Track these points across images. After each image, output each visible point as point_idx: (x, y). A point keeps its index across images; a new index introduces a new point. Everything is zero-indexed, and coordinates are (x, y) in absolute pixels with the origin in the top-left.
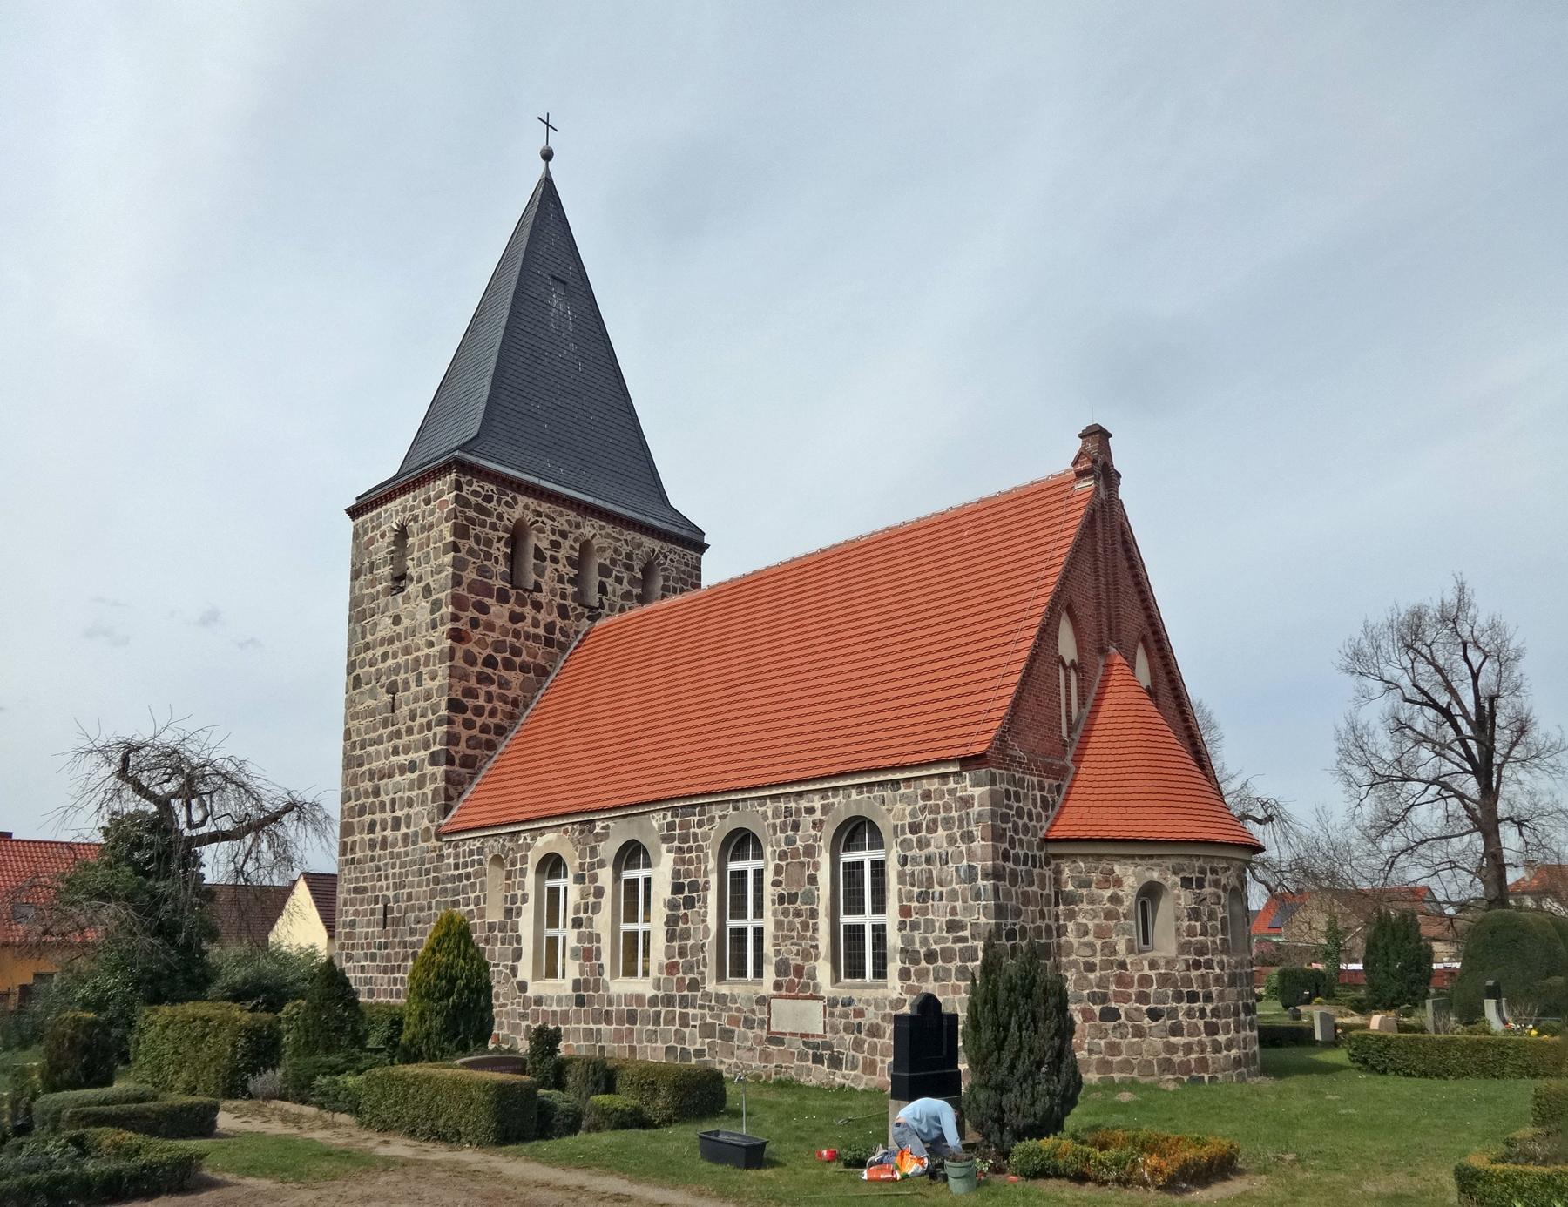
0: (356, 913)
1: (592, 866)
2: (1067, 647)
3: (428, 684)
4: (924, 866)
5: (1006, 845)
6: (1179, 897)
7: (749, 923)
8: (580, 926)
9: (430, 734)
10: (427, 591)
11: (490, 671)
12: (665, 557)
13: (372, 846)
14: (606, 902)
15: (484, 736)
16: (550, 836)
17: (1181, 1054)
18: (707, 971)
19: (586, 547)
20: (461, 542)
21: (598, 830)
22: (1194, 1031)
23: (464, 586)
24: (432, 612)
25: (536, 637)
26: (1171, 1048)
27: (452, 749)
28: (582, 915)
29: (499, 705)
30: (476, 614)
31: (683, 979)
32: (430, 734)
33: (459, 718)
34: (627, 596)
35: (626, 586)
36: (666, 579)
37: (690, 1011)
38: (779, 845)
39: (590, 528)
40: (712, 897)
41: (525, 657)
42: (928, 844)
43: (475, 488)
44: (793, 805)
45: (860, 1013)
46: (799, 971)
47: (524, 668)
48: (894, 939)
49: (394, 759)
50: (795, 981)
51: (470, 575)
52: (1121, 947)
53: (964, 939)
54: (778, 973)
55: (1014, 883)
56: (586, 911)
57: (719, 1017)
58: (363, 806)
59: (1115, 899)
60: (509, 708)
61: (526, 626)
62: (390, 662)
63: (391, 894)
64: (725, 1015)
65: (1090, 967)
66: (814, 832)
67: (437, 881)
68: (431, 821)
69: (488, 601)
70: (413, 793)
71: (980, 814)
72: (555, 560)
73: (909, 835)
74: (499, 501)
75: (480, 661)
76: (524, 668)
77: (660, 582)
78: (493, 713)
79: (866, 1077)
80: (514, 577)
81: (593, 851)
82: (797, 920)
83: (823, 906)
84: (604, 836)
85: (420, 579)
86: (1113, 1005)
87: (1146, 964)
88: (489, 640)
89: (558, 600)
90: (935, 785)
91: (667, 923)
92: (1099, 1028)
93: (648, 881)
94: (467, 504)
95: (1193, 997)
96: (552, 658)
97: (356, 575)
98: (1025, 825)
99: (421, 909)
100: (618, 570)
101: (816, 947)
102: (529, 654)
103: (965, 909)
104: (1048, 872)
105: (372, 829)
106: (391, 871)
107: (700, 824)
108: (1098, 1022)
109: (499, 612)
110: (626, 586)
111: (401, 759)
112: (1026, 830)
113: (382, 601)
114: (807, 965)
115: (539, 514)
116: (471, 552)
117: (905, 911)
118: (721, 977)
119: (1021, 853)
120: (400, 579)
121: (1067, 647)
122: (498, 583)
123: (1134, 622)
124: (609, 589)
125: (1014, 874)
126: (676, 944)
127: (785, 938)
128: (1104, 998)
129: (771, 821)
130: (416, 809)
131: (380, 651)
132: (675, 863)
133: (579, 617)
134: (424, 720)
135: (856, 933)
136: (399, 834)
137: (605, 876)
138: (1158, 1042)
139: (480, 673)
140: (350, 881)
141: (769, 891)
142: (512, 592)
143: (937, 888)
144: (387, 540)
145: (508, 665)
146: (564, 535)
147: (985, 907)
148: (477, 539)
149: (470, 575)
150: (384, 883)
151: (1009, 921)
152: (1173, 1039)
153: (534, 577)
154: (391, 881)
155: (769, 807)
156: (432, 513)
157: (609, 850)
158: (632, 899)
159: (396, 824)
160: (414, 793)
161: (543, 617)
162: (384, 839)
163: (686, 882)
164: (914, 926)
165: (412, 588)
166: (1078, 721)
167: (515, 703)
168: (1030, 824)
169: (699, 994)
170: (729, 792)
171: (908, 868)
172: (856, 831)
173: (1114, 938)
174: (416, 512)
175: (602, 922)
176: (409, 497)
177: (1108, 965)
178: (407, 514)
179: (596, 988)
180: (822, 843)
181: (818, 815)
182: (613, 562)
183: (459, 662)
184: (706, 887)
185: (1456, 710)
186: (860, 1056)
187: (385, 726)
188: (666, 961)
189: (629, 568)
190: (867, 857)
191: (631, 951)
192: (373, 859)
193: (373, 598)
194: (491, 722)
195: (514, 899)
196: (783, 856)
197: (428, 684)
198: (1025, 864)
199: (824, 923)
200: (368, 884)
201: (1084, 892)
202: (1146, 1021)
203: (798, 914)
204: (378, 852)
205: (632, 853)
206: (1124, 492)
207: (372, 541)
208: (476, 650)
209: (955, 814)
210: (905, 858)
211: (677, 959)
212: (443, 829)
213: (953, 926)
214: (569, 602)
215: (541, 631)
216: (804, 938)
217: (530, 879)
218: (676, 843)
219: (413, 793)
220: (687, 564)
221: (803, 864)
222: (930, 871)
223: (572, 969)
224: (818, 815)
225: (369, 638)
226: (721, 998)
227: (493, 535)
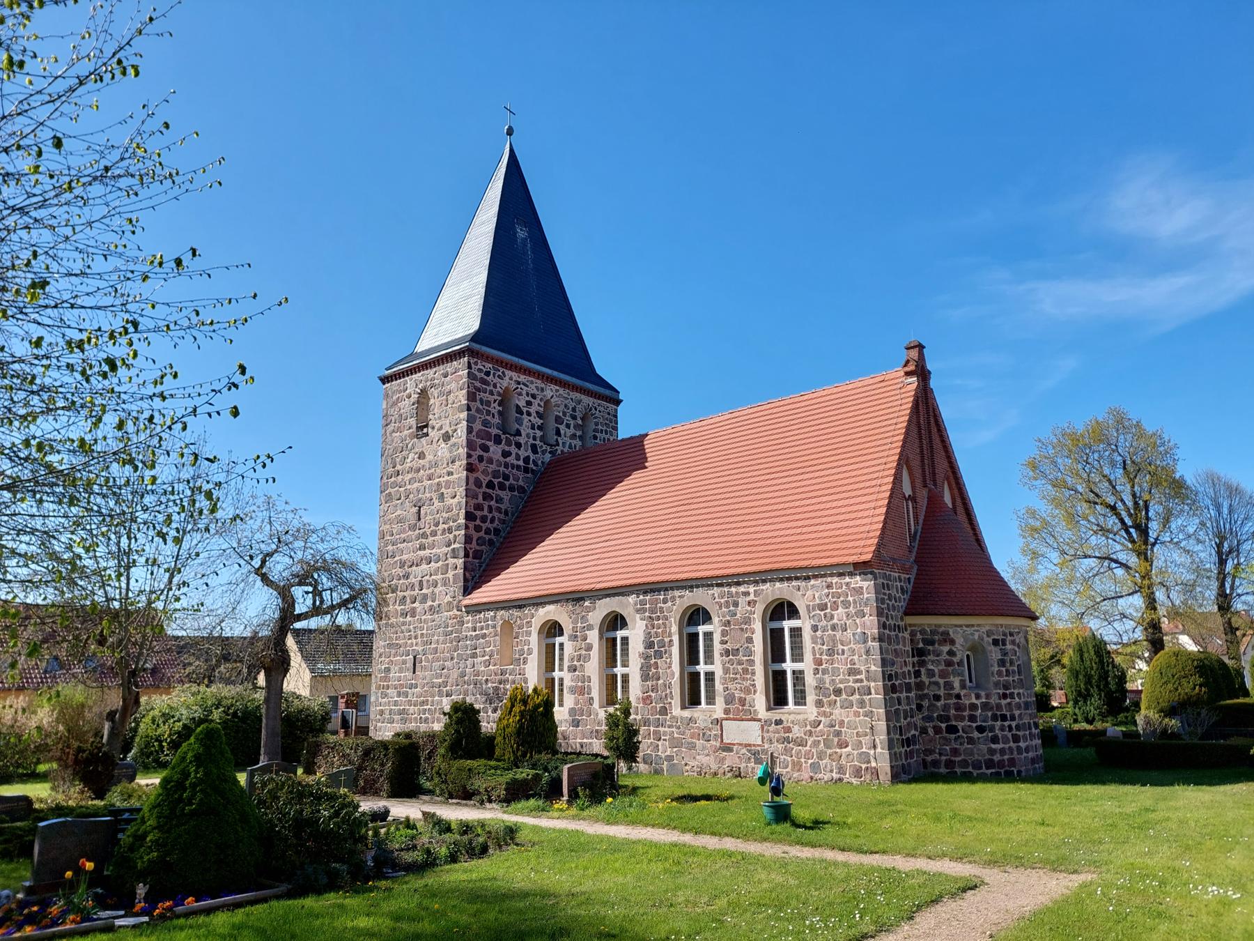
9: (451, 536)
11: (490, 491)
14: (595, 654)
15: (487, 537)
22: (1006, 741)
25: (518, 467)
26: (992, 752)
27: (468, 546)
29: (496, 514)
30: (482, 453)
32: (451, 536)
33: (471, 525)
35: (572, 430)
36: (597, 424)
40: (675, 650)
45: (789, 730)
46: (742, 702)
47: (512, 489)
48: (810, 680)
49: (422, 553)
50: (739, 710)
52: (957, 685)
53: (861, 681)
54: (727, 703)
55: (890, 644)
56: (579, 660)
59: (951, 653)
60: (502, 516)
63: (420, 649)
65: (937, 698)
72: (529, 414)
76: (512, 489)
78: (492, 521)
80: (504, 428)
82: (739, 667)
88: (490, 470)
89: (531, 441)
90: (835, 580)
92: (945, 738)
95: (1004, 718)
101: (754, 685)
107: (665, 601)
108: (945, 734)
109: (495, 451)
110: (572, 430)
111: (427, 552)
115: (519, 383)
117: (818, 662)
118: (683, 707)
120: (422, 429)
122: (494, 431)
123: (941, 465)
128: (947, 719)
134: (446, 526)
137: (593, 636)
138: (984, 748)
139: (484, 493)
141: (717, 647)
144: (412, 400)
146: (534, 396)
149: (478, 426)
152: (993, 746)
161: (523, 453)
164: (825, 672)
166: (916, 533)
171: (819, 633)
173: (952, 678)
177: (949, 696)
181: (752, 597)
185: (1120, 505)
189: (574, 418)
199: (759, 668)
201: (930, 648)
202: (976, 734)
203: (740, 663)
204: (409, 618)
206: (933, 384)
208: (482, 477)
209: (850, 599)
213: (852, 672)
214: (538, 442)
215: (521, 463)
217: (534, 638)
225: (399, 467)
227: (491, 398)
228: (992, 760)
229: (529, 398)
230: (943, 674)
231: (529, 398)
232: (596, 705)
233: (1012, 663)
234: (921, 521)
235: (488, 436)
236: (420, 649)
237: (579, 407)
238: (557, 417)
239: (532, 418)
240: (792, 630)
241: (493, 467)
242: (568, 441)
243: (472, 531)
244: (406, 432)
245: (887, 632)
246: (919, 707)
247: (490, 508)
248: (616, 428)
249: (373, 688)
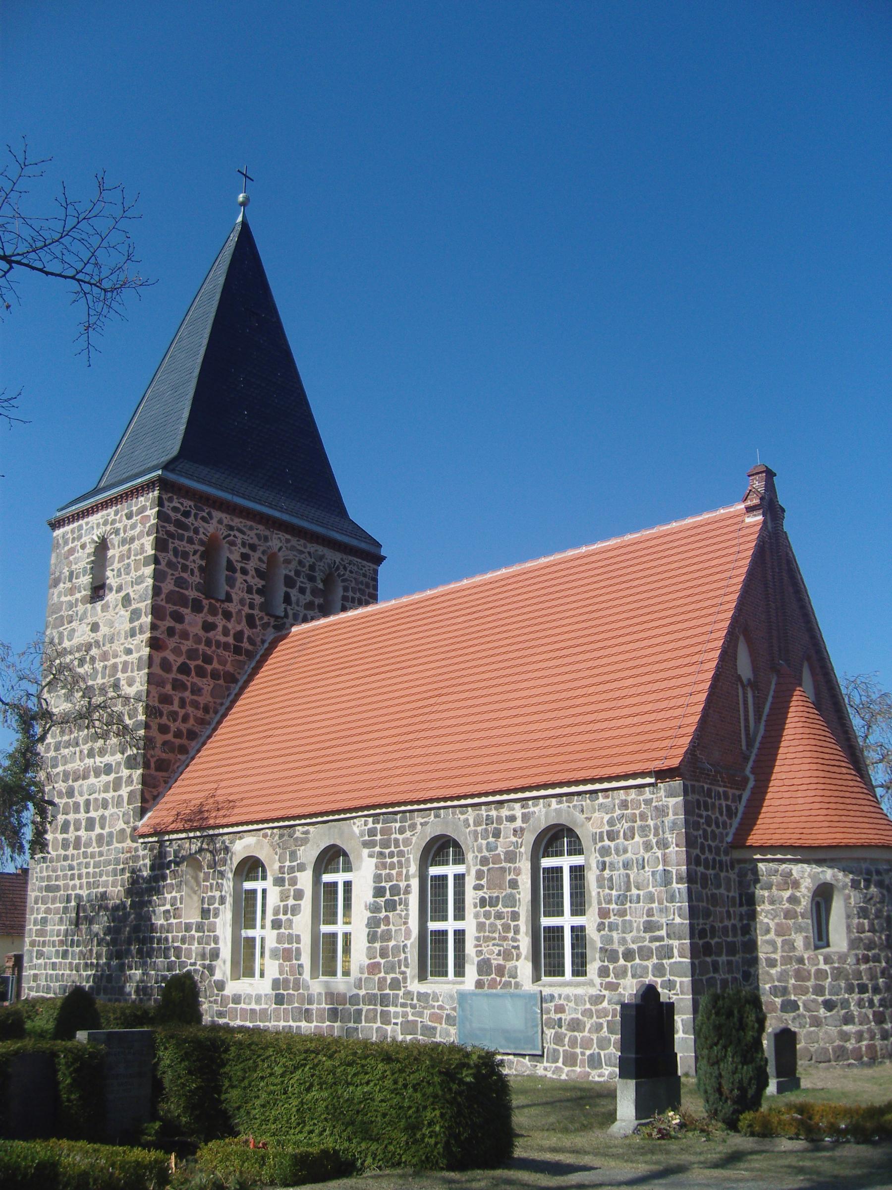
1: (292, 870)
4: (622, 871)
5: (698, 851)
6: (849, 897)
7: (450, 925)
8: (279, 927)
12: (345, 568)
13: (65, 845)
14: (306, 904)
15: (178, 741)
17: (853, 1041)
18: (408, 971)
19: (272, 559)
20: (161, 555)
21: (298, 834)
22: (864, 1020)
23: (163, 596)
24: (131, 621)
25: (226, 646)
26: (845, 1036)
28: (281, 917)
29: (190, 710)
31: (385, 979)
34: (309, 606)
35: (308, 597)
36: (346, 589)
37: (392, 1009)
38: (480, 850)
39: (277, 541)
42: (625, 851)
44: (494, 813)
46: (500, 971)
47: (215, 675)
49: (89, 762)
53: (661, 939)
54: (480, 972)
55: (704, 886)
57: (421, 1015)
59: (793, 900)
60: (200, 714)
61: (217, 635)
64: (427, 1012)
66: (514, 839)
68: (127, 823)
70: (109, 796)
71: (674, 823)
72: (244, 572)
73: (607, 842)
74: (196, 516)
75: (175, 668)
76: (215, 675)
77: (340, 592)
78: (185, 719)
79: (566, 1069)
80: (208, 588)
81: (293, 856)
82: (499, 923)
83: (524, 909)
84: (304, 841)
85: (119, 589)
86: (793, 997)
87: (821, 958)
88: (184, 649)
89: (246, 610)
90: (633, 794)
91: (368, 925)
93: (348, 885)
96: (240, 665)
98: (713, 831)
100: (301, 581)
101: (517, 948)
102: (220, 663)
103: (661, 910)
106: (84, 871)
107: (402, 831)
108: (779, 1013)
109: (193, 622)
110: (308, 597)
112: (714, 836)
113: (81, 608)
114: (509, 965)
115: (231, 528)
117: (604, 914)
118: (422, 977)
119: (710, 857)
120: (98, 591)
122: (192, 594)
124: (294, 599)
126: (377, 945)
127: (487, 939)
128: (784, 991)
129: (472, 828)
130: (111, 810)
132: (377, 867)
133: (265, 626)
135: (556, 933)
136: (93, 835)
137: (305, 880)
138: (833, 1030)
139: (175, 680)
140: (42, 879)
141: (471, 896)
143: (634, 891)
145: (201, 673)
146: (253, 547)
147: (680, 908)
148: (176, 552)
149: (168, 586)
150: (77, 882)
151: (701, 921)
152: (845, 1028)
153: (227, 588)
154: (84, 880)
155: (471, 814)
156: (133, 527)
157: (309, 854)
158: (329, 902)
162: (78, 839)
163: (387, 885)
165: (111, 597)
167: (206, 710)
168: (717, 831)
169: (401, 993)
170: (431, 800)
171: (607, 873)
172: (555, 838)
173: (793, 936)
174: (117, 525)
175: (302, 923)
176: (111, 511)
178: (109, 527)
179: (297, 987)
180: (523, 850)
181: (519, 823)
182: (297, 573)
184: (407, 891)
186: (561, 1049)
188: (367, 962)
189: (312, 579)
190: (565, 862)
191: (327, 953)
192: (66, 858)
193: (71, 605)
196: (484, 861)
198: (714, 868)
199: (524, 923)
200: (61, 883)
203: (499, 916)
204: (71, 851)
205: (332, 857)
206: (788, 526)
207: (72, 551)
208: (171, 657)
209: (651, 823)
210: (604, 863)
211: (378, 959)
212: (141, 830)
213: (649, 927)
214: (256, 612)
215: (230, 640)
216: (505, 939)
218: (377, 849)
219: (109, 796)
220: (365, 575)
221: (503, 869)
222: (628, 876)
223: (273, 968)
226: (422, 997)
227: (190, 548)
228: (842, 1049)
232: (307, 975)
235: (183, 601)
237: (320, 565)
238: (287, 577)
239: (249, 578)
240: (573, 869)
243: (154, 732)
244: (78, 596)
245: (701, 869)
249: (27, 947)
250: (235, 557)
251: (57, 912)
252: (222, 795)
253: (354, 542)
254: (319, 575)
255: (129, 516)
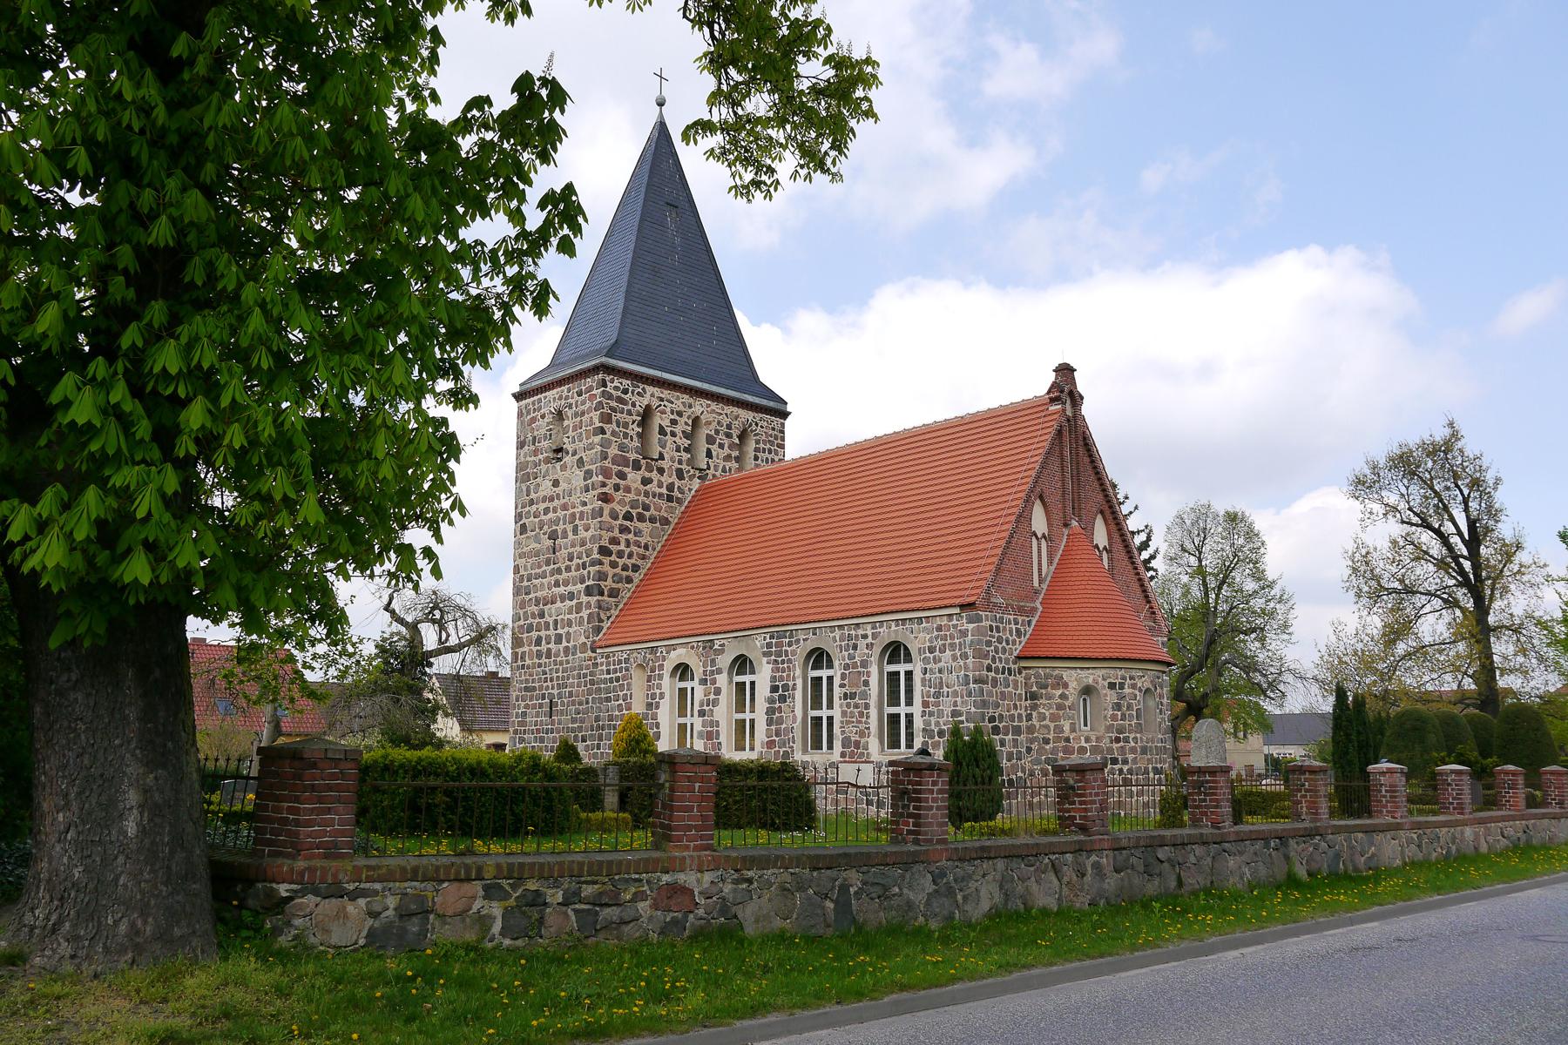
0: (527, 706)
1: (712, 672)
2: (1039, 522)
3: (582, 534)
10: (580, 462)
11: (628, 523)
13: (539, 655)
15: (625, 573)
16: (681, 651)
19: (696, 421)
20: (606, 427)
25: (661, 495)
29: (634, 549)
33: (606, 560)
35: (727, 450)
36: (757, 442)
39: (700, 407)
40: (798, 694)
41: (653, 511)
43: (615, 383)
46: (857, 745)
47: (653, 520)
48: (918, 723)
51: (613, 451)
52: (1067, 728)
58: (531, 625)
60: (641, 551)
62: (551, 515)
63: (555, 692)
65: (1047, 741)
67: (592, 682)
69: (626, 470)
72: (673, 434)
76: (653, 520)
78: (630, 556)
80: (644, 450)
81: (713, 661)
83: (873, 702)
84: (721, 652)
85: (574, 453)
89: (676, 465)
93: (753, 683)
94: (610, 397)
97: (521, 445)
99: (580, 704)
100: (721, 438)
104: (1020, 678)
105: (538, 642)
109: (634, 478)
110: (727, 450)
111: (561, 589)
113: (544, 467)
115: (662, 400)
116: (614, 433)
117: (925, 704)
118: (805, 751)
121: (1039, 522)
122: (633, 456)
125: (995, 681)
127: (848, 722)
131: (542, 506)
133: (691, 478)
136: (561, 647)
137: (722, 680)
141: (837, 691)
142: (643, 462)
145: (641, 518)
146: (680, 414)
149: (613, 451)
155: (837, 633)
156: (583, 403)
157: (725, 661)
159: (559, 639)
160: (572, 620)
161: (666, 480)
162: (549, 650)
165: (567, 459)
167: (646, 547)
172: (896, 651)
176: (565, 388)
177: (1058, 739)
181: (870, 640)
182: (717, 432)
183: (606, 517)
187: (548, 564)
189: (729, 436)
190: (902, 668)
192: (540, 665)
194: (629, 562)
195: (653, 696)
196: (847, 667)
197: (582, 534)
199: (873, 712)
203: (856, 706)
205: (742, 664)
206: (1086, 410)
207: (533, 420)
208: (618, 508)
214: (683, 467)
215: (664, 491)
224: (870, 640)
225: (533, 496)
227: (629, 419)
229: (674, 417)
230: (1054, 718)
231: (674, 417)
233: (1129, 707)
234: (1056, 561)
236: (555, 692)
241: (632, 496)
242: (722, 463)
246: (1029, 750)
247: (628, 541)
248: (782, 447)
250: (665, 423)
251: (534, 707)
252: (1351, 547)
253: (764, 402)
254: (735, 433)
255: (580, 394)
